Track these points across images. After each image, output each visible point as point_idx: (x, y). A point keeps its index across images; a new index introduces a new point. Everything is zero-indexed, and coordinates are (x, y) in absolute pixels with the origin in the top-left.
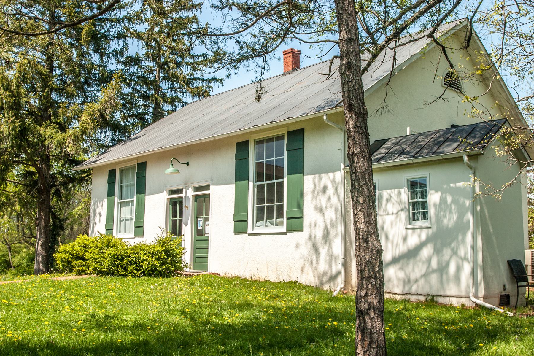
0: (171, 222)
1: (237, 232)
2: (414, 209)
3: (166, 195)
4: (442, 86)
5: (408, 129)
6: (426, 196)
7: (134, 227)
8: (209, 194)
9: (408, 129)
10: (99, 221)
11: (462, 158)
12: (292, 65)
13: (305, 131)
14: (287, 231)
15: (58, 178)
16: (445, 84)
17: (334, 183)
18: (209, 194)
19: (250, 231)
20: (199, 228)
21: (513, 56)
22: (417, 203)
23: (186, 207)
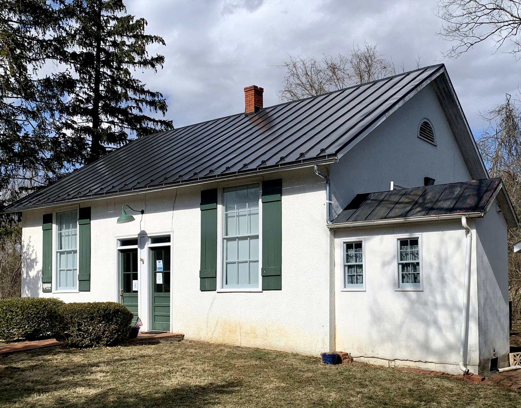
0: (123, 275)
1: (203, 289)
2: (403, 271)
3: (117, 246)
4: (418, 137)
5: (392, 183)
6: (418, 258)
7: (78, 281)
8: (169, 247)
9: (392, 183)
10: (36, 265)
11: (460, 220)
12: (255, 104)
13: (283, 181)
14: (263, 290)
15: (95, 42)
16: (420, 135)
17: (149, 98)
18: (169, 247)
19: (219, 289)
20: (157, 283)
21: (296, 80)
22: (407, 265)
23: (142, 260)
